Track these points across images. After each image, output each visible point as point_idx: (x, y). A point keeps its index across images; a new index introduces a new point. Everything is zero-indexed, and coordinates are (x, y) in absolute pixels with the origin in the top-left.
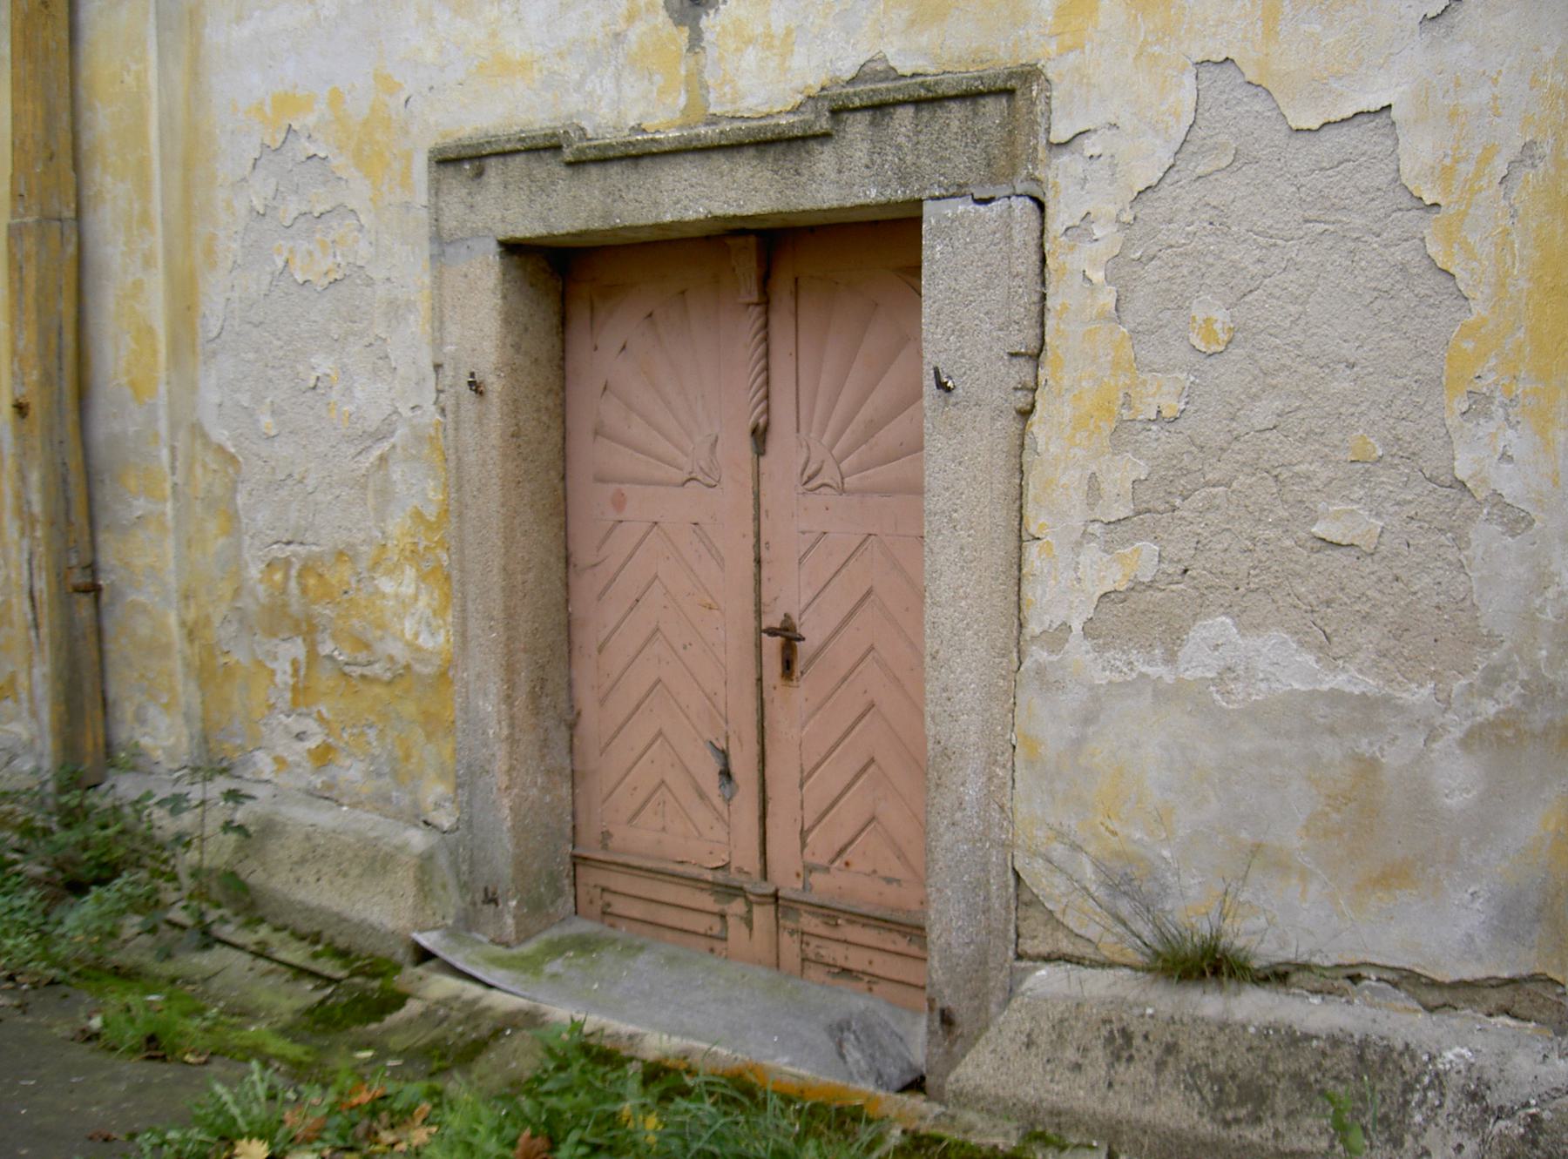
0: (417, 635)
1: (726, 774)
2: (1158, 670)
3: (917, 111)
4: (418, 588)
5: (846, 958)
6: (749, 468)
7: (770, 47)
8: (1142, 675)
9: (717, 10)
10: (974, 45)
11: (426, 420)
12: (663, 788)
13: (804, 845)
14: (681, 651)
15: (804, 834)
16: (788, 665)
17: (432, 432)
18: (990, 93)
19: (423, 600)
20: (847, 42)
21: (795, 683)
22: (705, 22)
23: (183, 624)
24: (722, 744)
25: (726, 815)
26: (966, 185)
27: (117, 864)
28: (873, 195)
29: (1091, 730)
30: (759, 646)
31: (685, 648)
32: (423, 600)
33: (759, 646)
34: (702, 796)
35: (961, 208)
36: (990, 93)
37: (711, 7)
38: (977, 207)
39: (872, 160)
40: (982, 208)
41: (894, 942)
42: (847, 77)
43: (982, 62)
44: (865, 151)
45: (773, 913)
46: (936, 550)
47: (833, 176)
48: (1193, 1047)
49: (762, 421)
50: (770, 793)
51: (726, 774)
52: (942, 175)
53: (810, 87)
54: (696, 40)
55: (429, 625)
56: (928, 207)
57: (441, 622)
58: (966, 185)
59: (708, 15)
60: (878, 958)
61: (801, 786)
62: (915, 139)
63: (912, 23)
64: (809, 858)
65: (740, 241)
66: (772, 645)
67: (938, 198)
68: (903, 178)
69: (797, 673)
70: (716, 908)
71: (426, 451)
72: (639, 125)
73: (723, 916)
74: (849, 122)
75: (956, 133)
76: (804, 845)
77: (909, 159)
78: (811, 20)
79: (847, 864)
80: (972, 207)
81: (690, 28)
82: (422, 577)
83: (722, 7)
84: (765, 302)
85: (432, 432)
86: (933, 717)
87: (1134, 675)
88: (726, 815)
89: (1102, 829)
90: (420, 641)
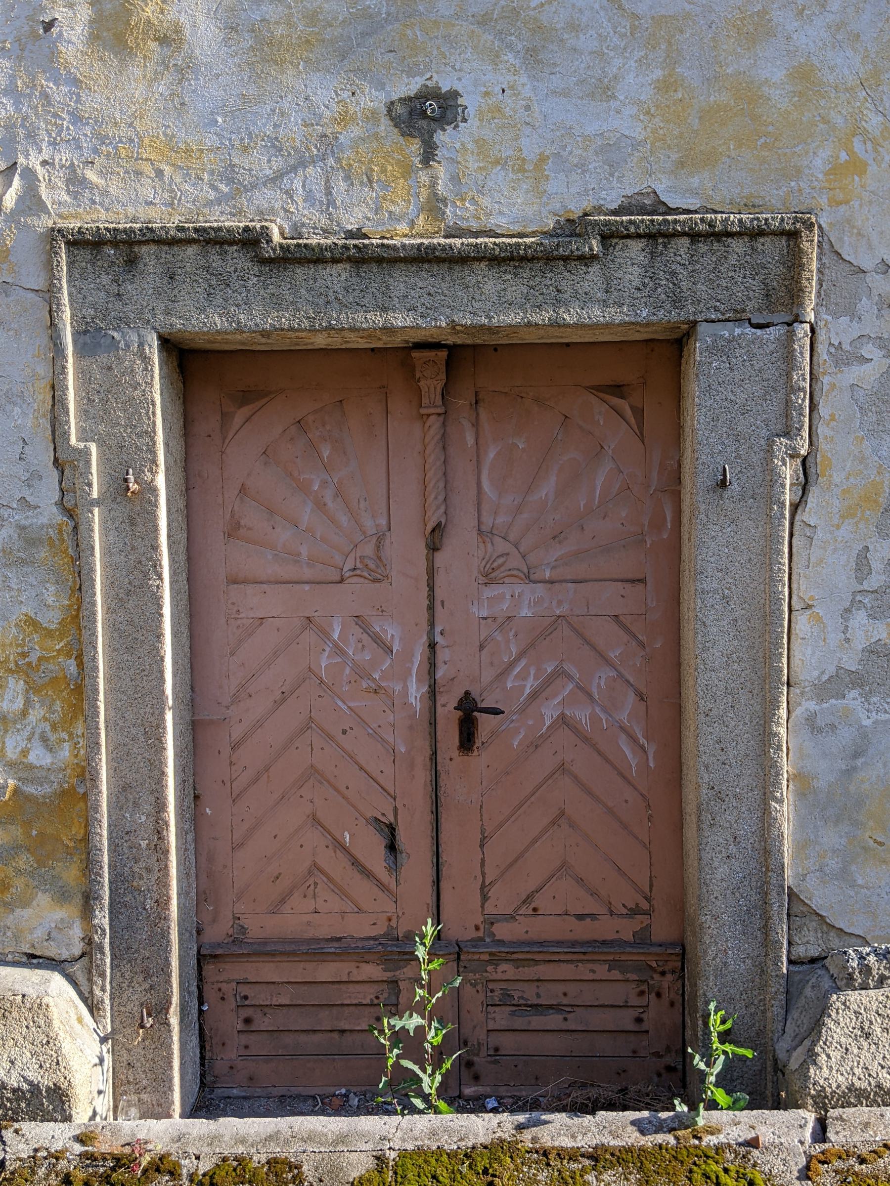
0: (25, 752)
3: (693, 242)
4: (28, 702)
5: (538, 996)
6: (423, 564)
7: (521, 170)
9: (457, 126)
10: (746, 191)
11: (45, 520)
13: (485, 898)
14: (340, 737)
17: (52, 533)
19: (36, 714)
20: (612, 175)
21: (476, 753)
25: (393, 886)
26: (744, 311)
28: (644, 314)
29: (859, 762)
31: (344, 732)
32: (36, 714)
34: (367, 873)
35: (738, 331)
37: (449, 124)
38: (753, 330)
39: (643, 284)
40: (759, 332)
41: (593, 971)
42: (614, 206)
43: (754, 206)
44: (636, 274)
45: (456, 966)
46: (708, 623)
47: (600, 295)
50: (444, 857)
52: (718, 301)
53: (570, 211)
55: (44, 739)
56: (702, 328)
57: (65, 736)
58: (744, 311)
59: (444, 130)
60: (571, 989)
61: (482, 846)
62: (691, 268)
63: (681, 164)
64: (489, 908)
65: (430, 354)
67: (713, 321)
68: (677, 301)
69: (478, 743)
70: (388, 975)
71: (43, 553)
72: (359, 229)
73: (395, 982)
74: (618, 248)
75: (734, 265)
76: (485, 898)
77: (685, 285)
78: (569, 149)
79: (535, 910)
80: (749, 330)
81: (423, 141)
82: (32, 688)
83: (461, 125)
85: (52, 533)
86: (707, 767)
88: (393, 886)
89: (871, 842)
90: (32, 758)
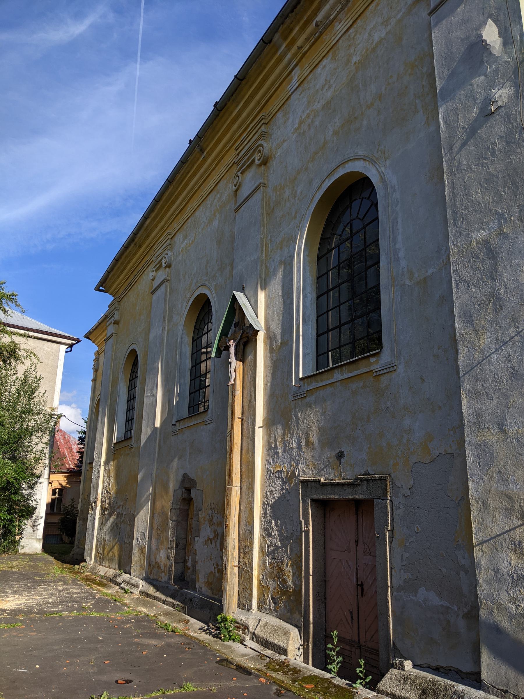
1: (352, 617)
2: (414, 598)
8: (411, 599)
12: (362, 218)
15: (366, 632)
16: (362, 595)
18: (393, 534)
22: (342, 460)
23: (293, 135)
24: (351, 611)
27: (148, 576)
30: (357, 588)
33: (357, 588)
36: (393, 534)
48: (418, 682)
49: (357, 539)
51: (352, 617)
54: (340, 462)
66: (359, 588)
70: (350, 649)
84: (357, 514)
87: (410, 599)
